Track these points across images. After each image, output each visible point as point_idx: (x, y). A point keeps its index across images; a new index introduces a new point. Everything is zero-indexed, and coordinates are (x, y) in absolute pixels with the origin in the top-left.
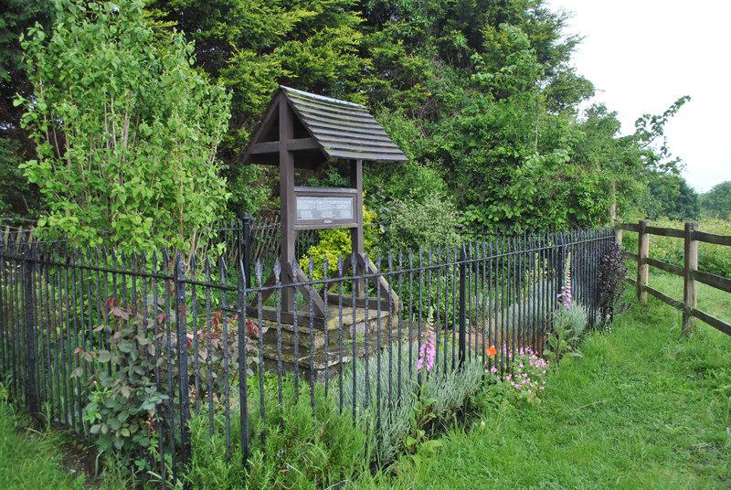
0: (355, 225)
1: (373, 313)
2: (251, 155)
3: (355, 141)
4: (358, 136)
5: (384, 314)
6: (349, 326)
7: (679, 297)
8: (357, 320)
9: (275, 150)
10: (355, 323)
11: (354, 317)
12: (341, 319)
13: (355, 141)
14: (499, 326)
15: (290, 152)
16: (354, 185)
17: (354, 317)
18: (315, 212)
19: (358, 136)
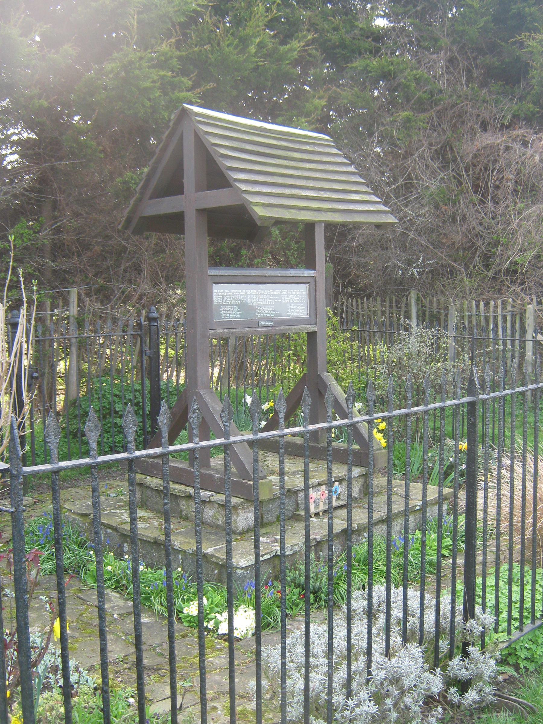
0: (312, 328)
1: (340, 471)
2: (141, 217)
3: (352, 207)
4: (311, 184)
5: (356, 471)
6: (296, 492)
7: (344, 512)
8: (312, 482)
9: (179, 210)
10: (307, 488)
11: (307, 479)
12: (282, 480)
13: (352, 207)
14: (518, 502)
15: (201, 211)
16: (311, 264)
17: (307, 479)
18: (243, 306)
19: (311, 184)
